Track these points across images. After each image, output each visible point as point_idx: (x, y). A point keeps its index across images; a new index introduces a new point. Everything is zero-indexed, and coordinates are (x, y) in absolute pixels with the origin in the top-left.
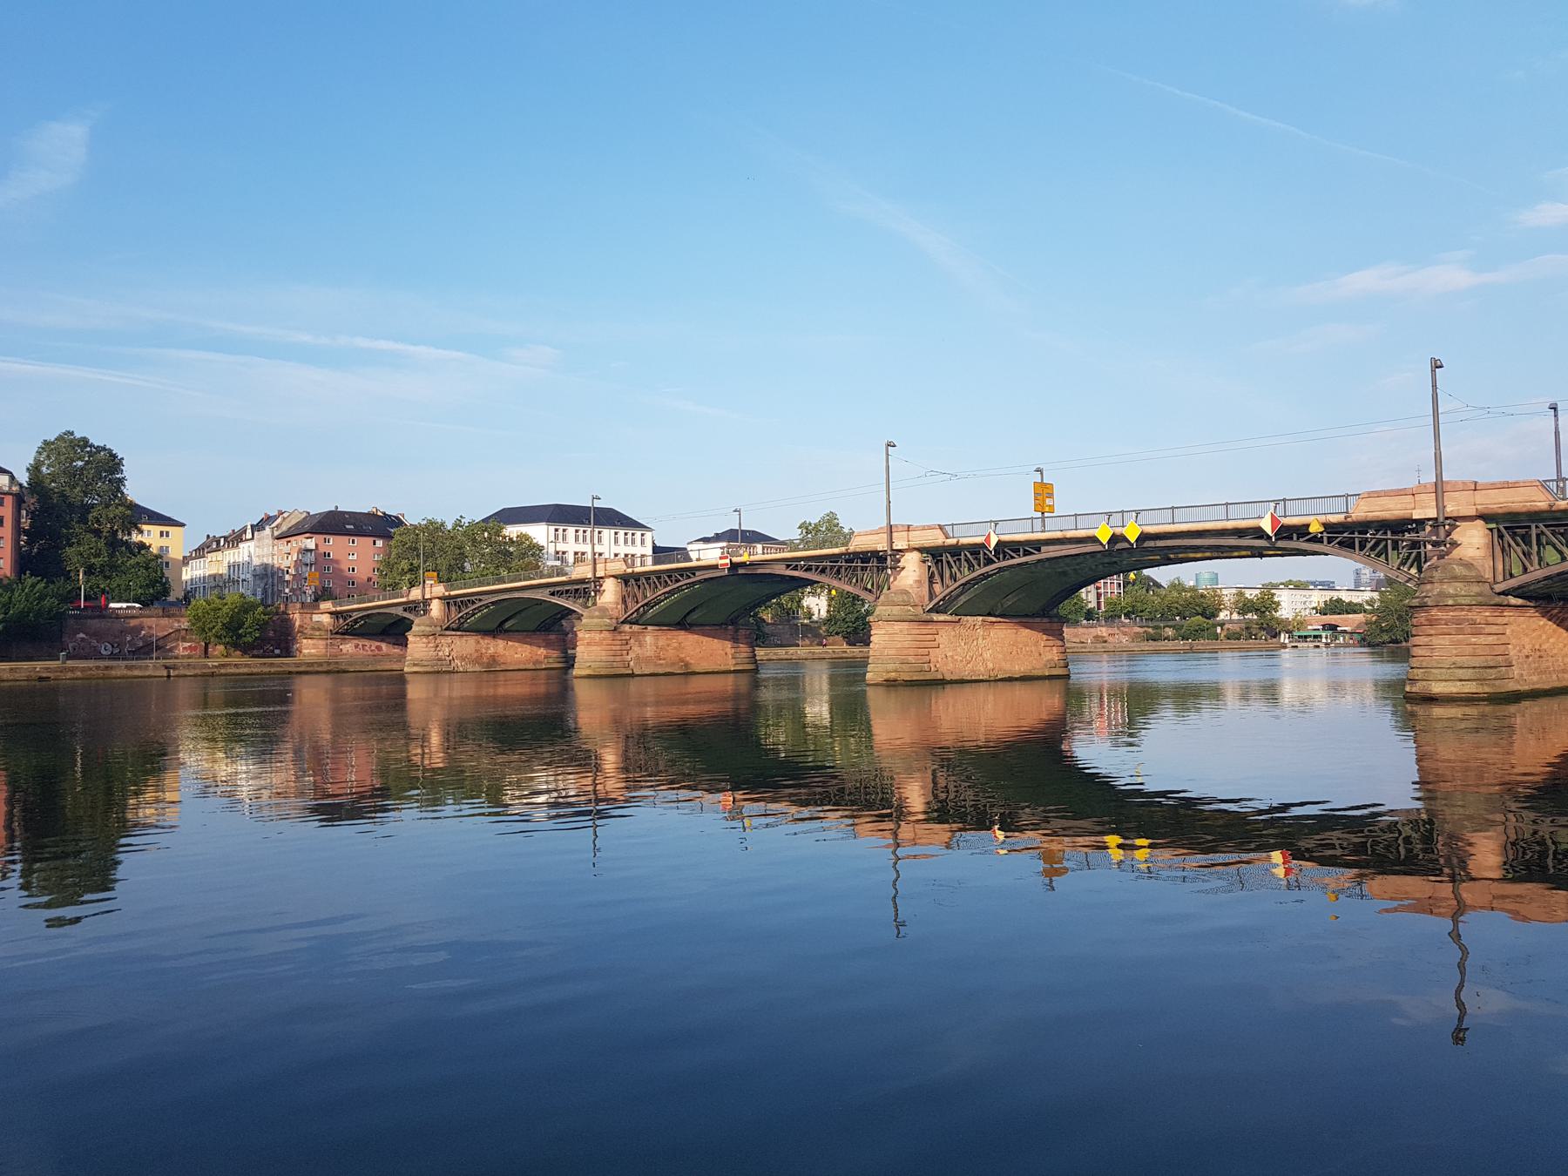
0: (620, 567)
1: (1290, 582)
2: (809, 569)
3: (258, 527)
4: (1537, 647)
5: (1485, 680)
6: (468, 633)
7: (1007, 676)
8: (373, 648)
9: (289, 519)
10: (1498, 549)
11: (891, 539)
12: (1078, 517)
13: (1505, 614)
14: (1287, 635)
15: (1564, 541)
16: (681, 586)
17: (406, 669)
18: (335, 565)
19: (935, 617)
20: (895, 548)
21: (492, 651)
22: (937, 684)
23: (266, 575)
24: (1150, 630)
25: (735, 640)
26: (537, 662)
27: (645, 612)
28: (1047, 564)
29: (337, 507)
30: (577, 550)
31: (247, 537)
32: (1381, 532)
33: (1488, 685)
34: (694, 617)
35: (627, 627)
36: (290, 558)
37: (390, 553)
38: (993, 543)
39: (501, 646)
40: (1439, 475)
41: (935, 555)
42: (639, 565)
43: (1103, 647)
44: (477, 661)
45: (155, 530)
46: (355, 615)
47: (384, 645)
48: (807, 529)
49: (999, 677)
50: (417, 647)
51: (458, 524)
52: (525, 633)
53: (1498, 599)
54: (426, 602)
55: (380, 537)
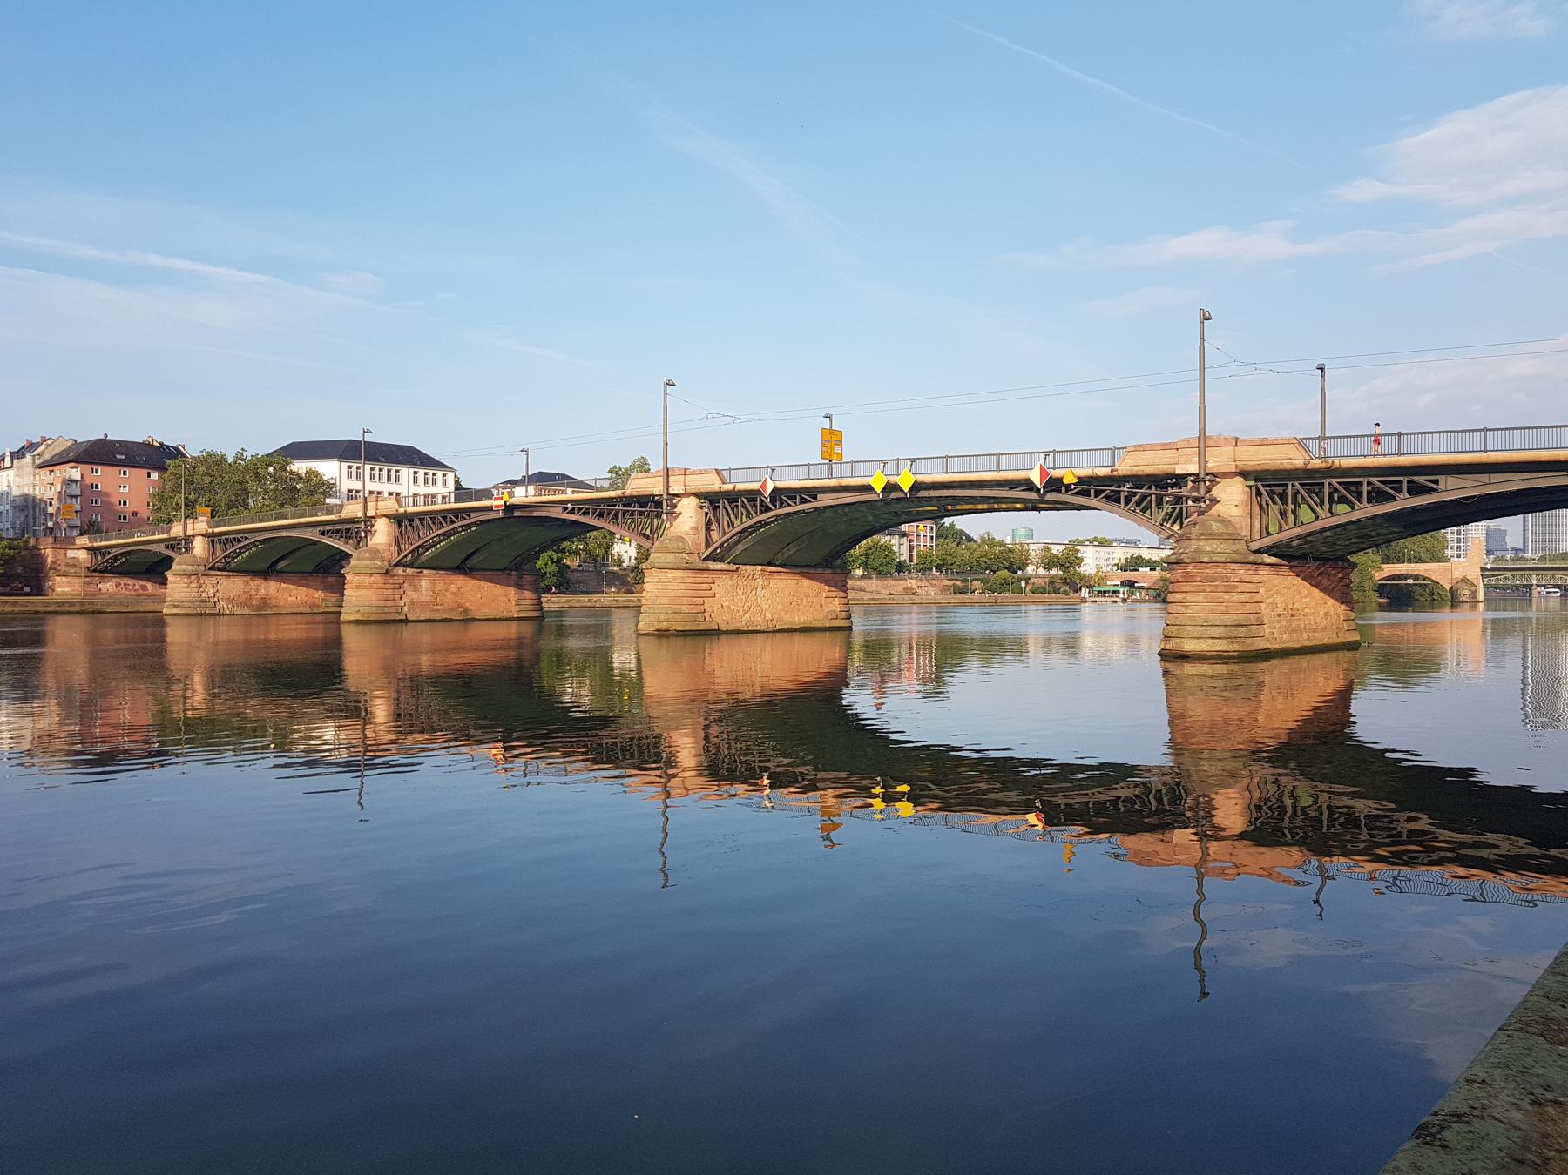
0: (390, 506)
1: (1095, 539)
2: (586, 513)
3: (18, 455)
4: (1290, 606)
6: (236, 574)
7: (786, 627)
8: (137, 587)
9: (53, 446)
10: (1256, 509)
11: (668, 482)
13: (1260, 572)
14: (1087, 590)
15: (1318, 500)
16: (456, 528)
17: (165, 611)
18: (105, 499)
19: (712, 565)
20: (671, 492)
21: (262, 592)
22: (711, 635)
23: (27, 506)
24: (959, 583)
25: (519, 585)
26: (314, 605)
27: (419, 555)
28: (847, 509)
29: (106, 435)
30: (391, 491)
31: (6, 465)
32: (1146, 487)
34: (475, 560)
35: (400, 571)
36: (53, 488)
37: (164, 486)
38: (769, 490)
39: (273, 588)
40: (1202, 430)
41: (712, 500)
42: (422, 503)
43: (911, 599)
44: (246, 603)
46: (115, 552)
47: (149, 585)
48: (616, 473)
49: (778, 628)
50: (178, 587)
51: (240, 456)
52: (301, 575)
53: (1252, 558)
54: (188, 540)
55: (155, 469)
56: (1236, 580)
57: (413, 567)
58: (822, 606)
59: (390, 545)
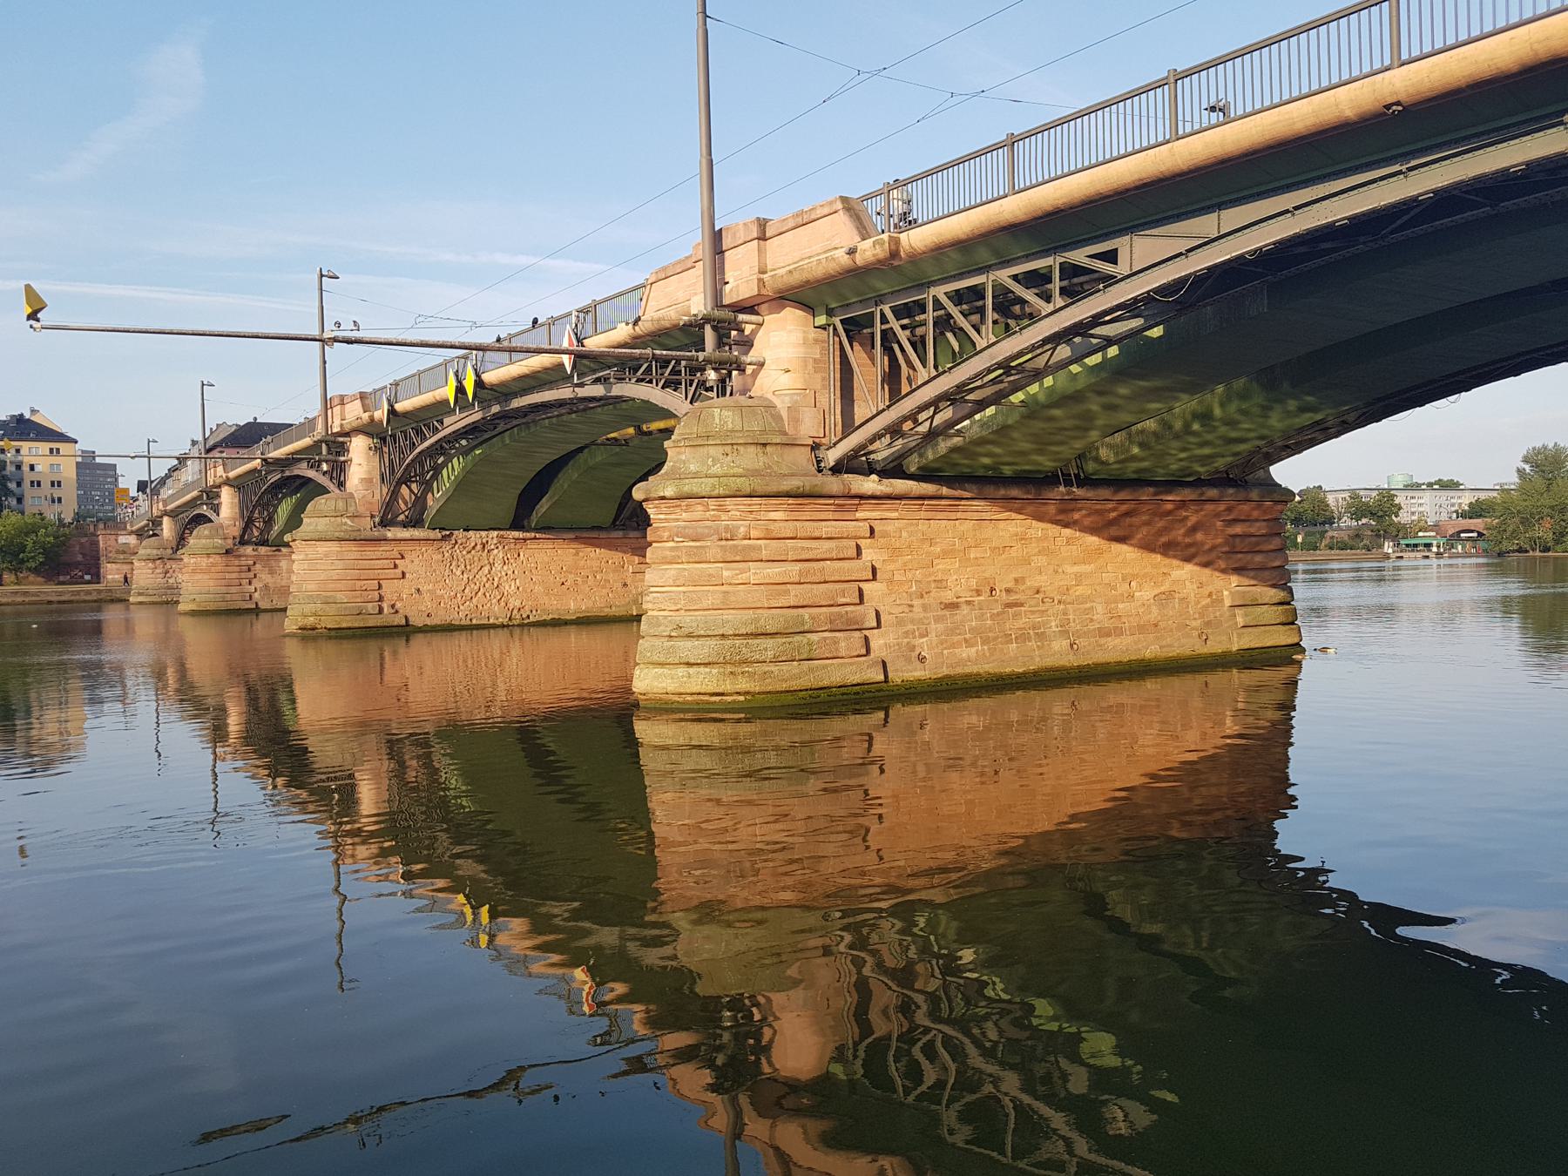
1: (1439, 482)
5: (745, 662)
12: (336, 352)
17: (131, 599)
29: (255, 419)
33: (751, 675)
35: (249, 550)
45: (44, 447)
49: (532, 619)
56: (753, 534)
57: (268, 546)
58: (625, 585)
59: (235, 519)
